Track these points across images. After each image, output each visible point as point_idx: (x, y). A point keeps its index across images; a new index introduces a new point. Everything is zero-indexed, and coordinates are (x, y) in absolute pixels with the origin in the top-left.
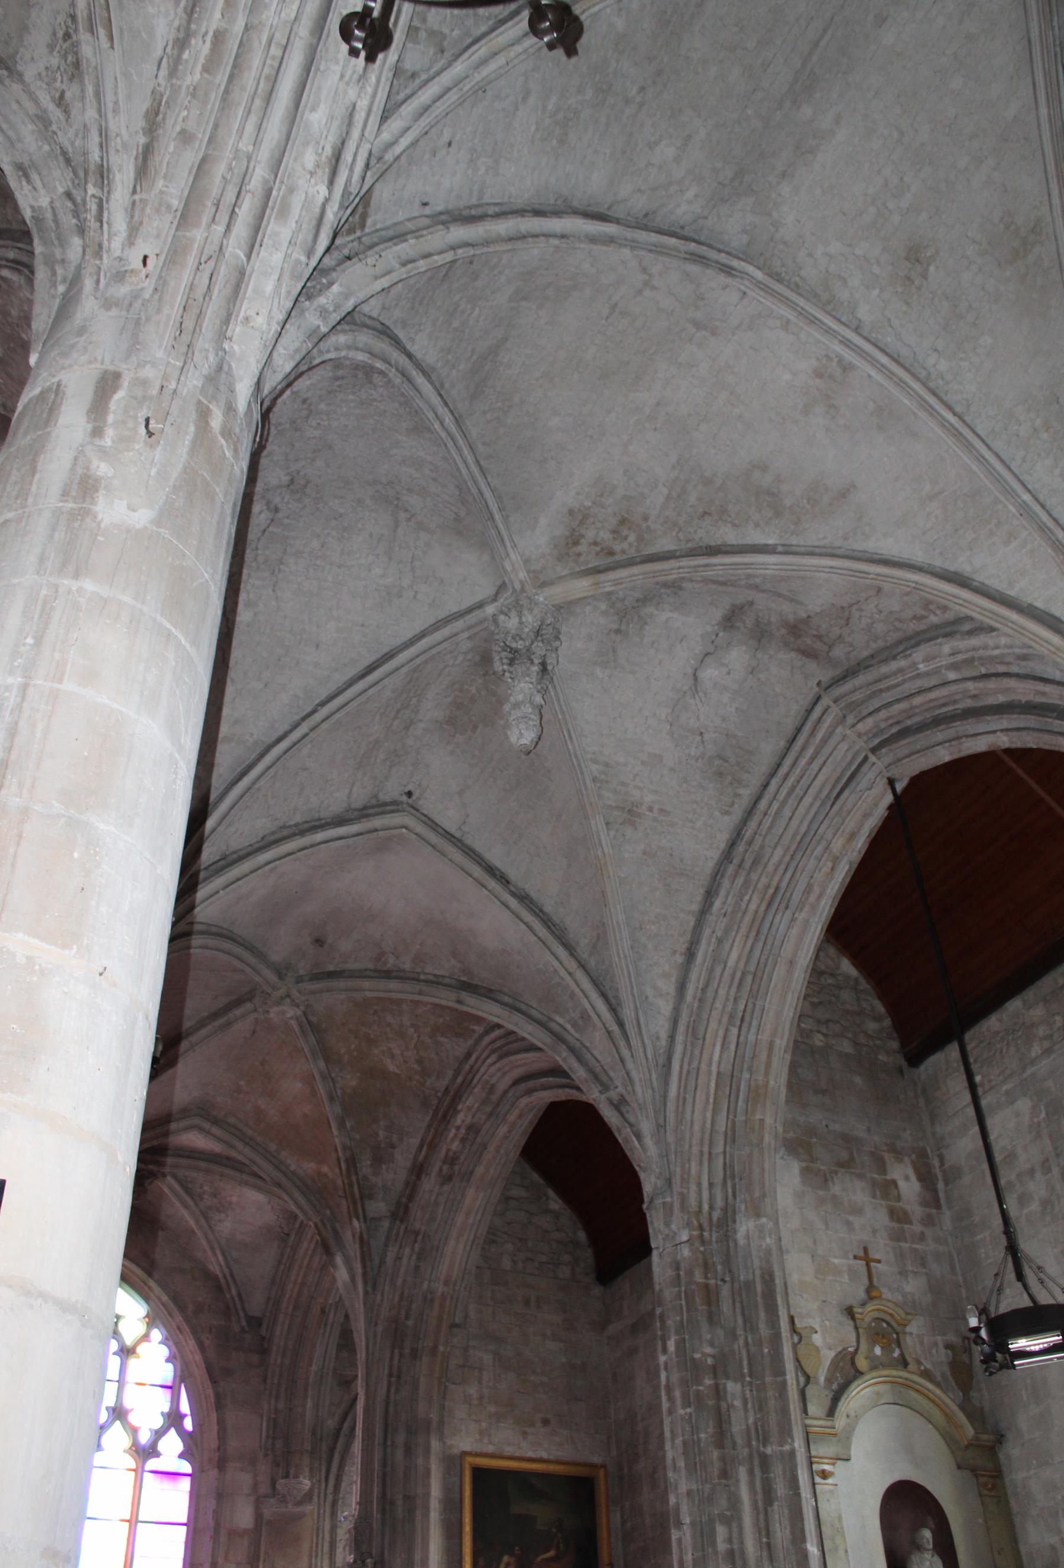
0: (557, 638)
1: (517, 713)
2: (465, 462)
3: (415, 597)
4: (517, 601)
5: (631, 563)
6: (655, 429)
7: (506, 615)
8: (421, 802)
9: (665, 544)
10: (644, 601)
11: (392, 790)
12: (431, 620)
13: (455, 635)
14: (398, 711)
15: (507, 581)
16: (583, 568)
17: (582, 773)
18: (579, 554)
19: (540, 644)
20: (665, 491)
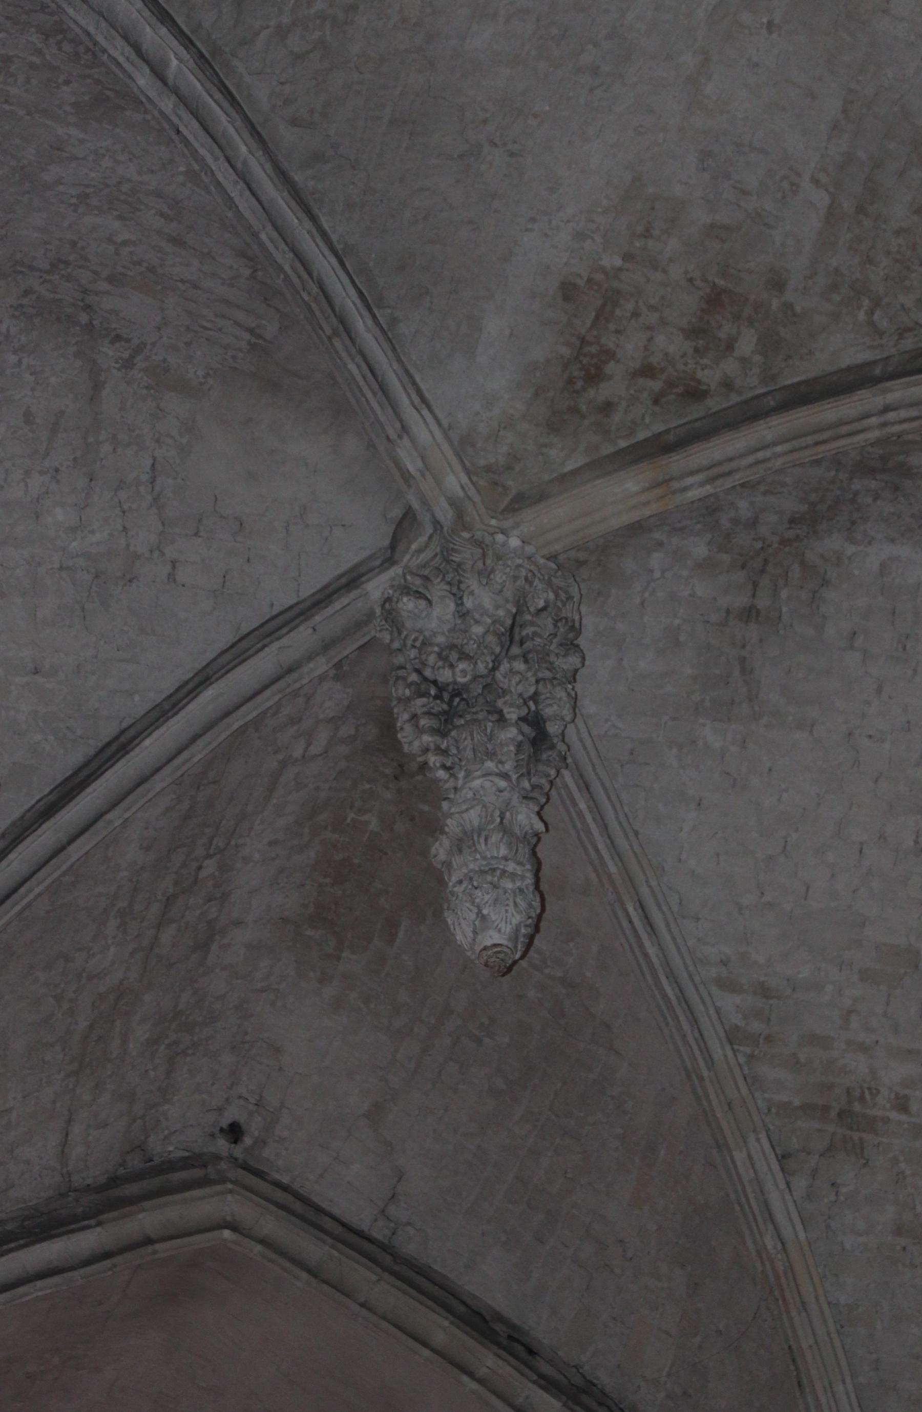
0: (571, 646)
1: (466, 864)
2: (244, 177)
3: (172, 577)
4: (446, 554)
5: (750, 413)
6: (770, 26)
7: (419, 595)
8: (266, 1153)
9: (840, 348)
10: (810, 520)
11: (183, 1125)
12: (227, 637)
13: (290, 670)
14: (169, 902)
15: (416, 505)
16: (623, 444)
17: (694, 1021)
18: (608, 407)
19: (520, 666)
20: (821, 198)
